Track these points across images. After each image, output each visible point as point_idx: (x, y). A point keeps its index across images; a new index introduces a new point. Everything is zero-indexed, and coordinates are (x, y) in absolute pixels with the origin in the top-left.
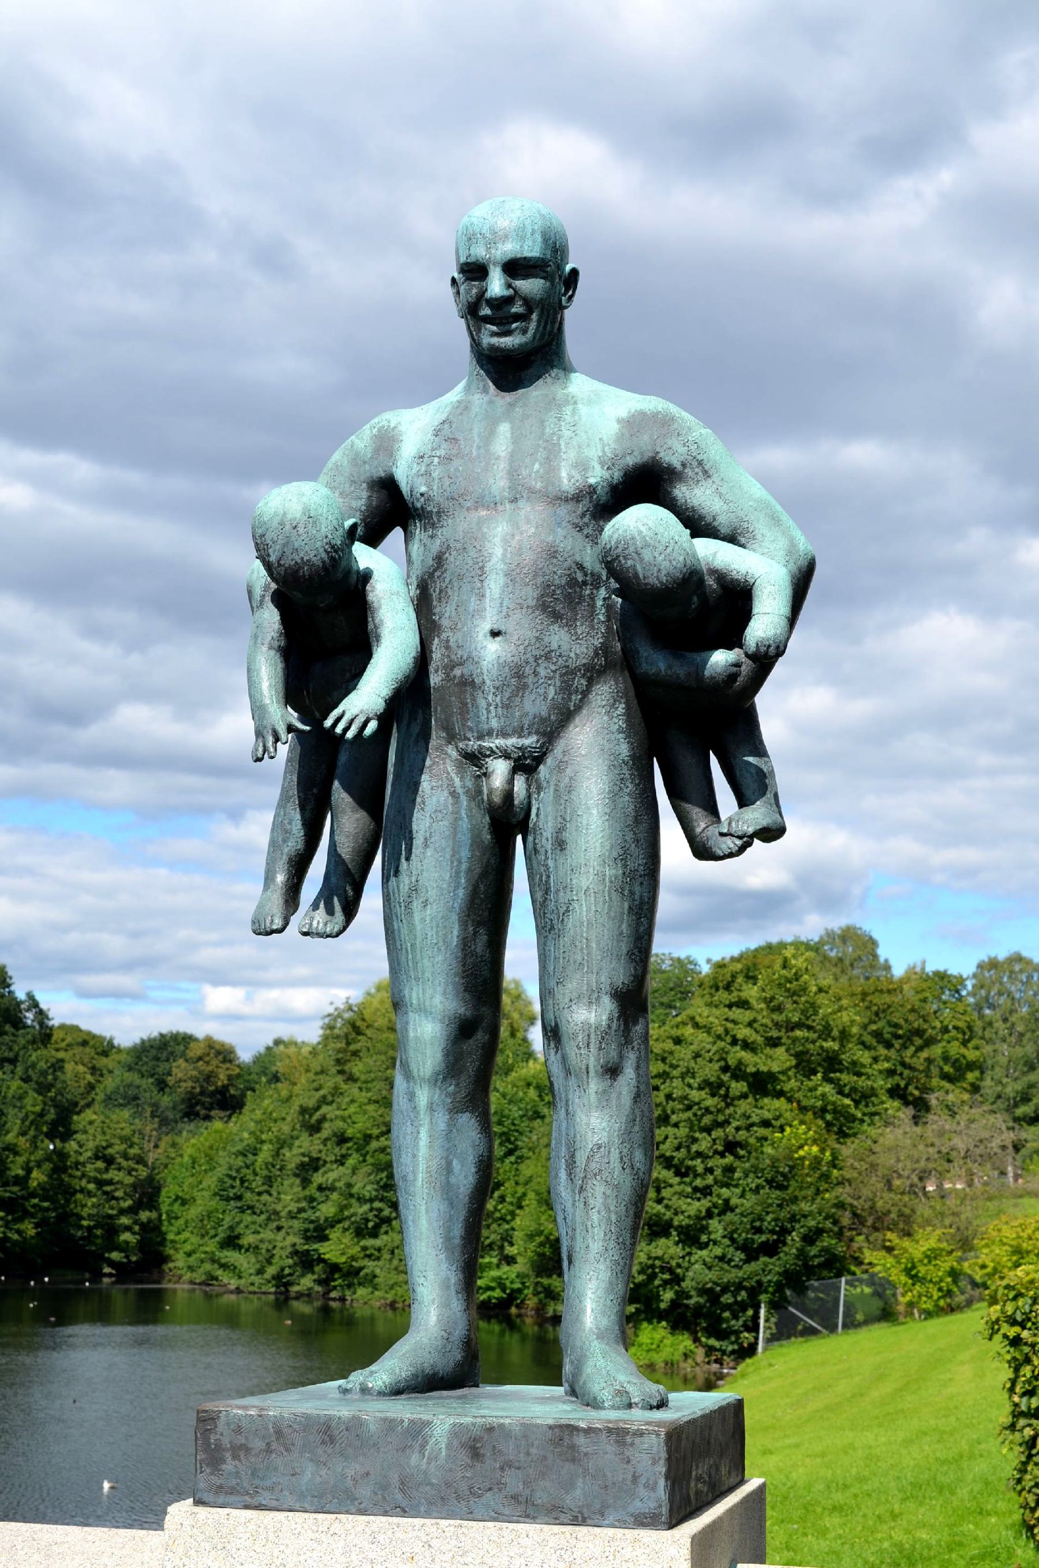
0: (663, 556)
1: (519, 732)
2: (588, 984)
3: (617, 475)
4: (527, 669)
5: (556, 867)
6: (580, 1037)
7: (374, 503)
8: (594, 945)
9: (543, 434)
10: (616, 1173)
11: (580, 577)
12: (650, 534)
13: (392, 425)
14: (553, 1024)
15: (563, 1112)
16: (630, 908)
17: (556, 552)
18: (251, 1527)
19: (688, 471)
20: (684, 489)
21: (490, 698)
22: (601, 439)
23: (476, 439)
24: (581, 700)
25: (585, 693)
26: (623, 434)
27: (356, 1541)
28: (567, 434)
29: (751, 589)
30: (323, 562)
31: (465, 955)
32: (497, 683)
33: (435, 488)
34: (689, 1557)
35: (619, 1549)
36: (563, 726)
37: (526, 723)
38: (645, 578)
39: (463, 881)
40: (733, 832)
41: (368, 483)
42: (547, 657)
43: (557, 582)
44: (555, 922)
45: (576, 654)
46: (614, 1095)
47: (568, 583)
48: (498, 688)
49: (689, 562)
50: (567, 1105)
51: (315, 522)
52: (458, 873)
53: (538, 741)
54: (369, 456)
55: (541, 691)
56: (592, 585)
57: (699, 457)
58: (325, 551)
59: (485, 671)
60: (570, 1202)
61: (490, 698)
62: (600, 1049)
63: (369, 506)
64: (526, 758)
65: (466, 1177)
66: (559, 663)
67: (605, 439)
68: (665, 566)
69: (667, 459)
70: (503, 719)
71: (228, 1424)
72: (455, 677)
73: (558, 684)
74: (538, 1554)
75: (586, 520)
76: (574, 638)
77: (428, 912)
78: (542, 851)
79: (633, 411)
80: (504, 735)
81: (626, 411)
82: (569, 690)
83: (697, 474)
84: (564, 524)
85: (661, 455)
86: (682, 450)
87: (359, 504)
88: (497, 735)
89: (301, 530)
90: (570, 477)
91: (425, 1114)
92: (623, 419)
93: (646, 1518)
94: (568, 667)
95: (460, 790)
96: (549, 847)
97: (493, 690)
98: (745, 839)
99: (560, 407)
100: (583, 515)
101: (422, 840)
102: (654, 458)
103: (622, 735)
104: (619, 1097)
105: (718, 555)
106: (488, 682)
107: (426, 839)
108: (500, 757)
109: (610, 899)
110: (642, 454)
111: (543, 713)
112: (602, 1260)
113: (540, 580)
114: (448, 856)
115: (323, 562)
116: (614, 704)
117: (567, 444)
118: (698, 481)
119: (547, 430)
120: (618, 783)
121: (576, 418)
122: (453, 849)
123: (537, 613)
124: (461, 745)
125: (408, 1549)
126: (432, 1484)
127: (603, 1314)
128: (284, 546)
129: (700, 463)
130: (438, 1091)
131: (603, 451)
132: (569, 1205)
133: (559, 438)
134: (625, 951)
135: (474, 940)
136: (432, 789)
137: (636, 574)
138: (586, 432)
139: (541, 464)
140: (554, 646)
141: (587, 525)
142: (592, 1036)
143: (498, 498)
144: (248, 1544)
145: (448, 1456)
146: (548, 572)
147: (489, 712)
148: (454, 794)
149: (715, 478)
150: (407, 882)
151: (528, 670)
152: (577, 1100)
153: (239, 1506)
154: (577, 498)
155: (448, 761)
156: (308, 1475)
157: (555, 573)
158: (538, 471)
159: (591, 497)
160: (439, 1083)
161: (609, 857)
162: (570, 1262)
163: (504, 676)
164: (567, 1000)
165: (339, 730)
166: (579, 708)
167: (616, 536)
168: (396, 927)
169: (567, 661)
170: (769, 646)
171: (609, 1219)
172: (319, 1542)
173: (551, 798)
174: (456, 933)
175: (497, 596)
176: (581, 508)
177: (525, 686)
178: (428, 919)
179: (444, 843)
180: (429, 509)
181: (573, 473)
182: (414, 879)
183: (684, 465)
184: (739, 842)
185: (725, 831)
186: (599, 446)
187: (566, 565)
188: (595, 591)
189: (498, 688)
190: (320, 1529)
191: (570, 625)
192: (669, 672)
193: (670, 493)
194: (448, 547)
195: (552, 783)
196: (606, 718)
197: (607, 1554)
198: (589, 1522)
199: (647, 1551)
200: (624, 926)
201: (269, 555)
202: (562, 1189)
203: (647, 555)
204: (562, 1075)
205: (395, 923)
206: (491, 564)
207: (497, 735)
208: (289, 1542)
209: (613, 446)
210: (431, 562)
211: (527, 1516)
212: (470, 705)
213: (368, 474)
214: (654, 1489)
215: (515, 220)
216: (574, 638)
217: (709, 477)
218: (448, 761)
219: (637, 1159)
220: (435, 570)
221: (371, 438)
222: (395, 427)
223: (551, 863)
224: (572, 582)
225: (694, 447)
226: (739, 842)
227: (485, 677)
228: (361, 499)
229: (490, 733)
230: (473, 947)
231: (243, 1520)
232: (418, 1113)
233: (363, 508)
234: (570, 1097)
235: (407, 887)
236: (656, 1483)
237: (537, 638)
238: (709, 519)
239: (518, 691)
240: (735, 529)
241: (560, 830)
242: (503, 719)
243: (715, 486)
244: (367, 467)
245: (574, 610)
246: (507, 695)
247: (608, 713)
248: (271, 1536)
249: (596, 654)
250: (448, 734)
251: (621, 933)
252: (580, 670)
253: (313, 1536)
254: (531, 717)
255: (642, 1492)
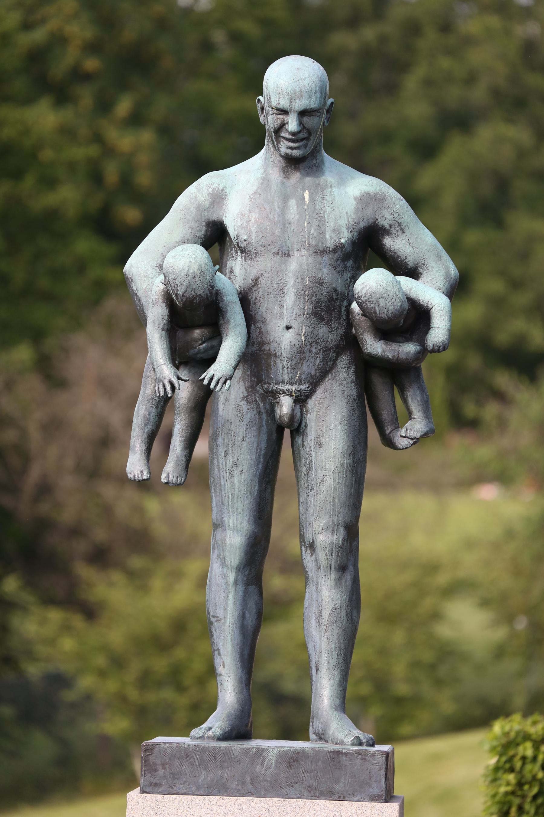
0: (390, 303)
1: (299, 382)
2: (333, 521)
3: (355, 235)
4: (306, 349)
5: (316, 457)
6: (328, 549)
7: (209, 234)
8: (336, 500)
9: (315, 209)
10: (344, 623)
11: (334, 296)
12: (384, 291)
13: (221, 188)
14: (311, 541)
15: (314, 589)
16: (356, 480)
17: (323, 282)
18: (176, 802)
19: (393, 230)
20: (390, 239)
21: (285, 363)
22: (346, 213)
23: (277, 209)
24: (333, 365)
25: (335, 361)
26: (358, 208)
27: (230, 809)
28: (328, 209)
29: (430, 311)
30: (207, 295)
31: (260, 500)
32: (289, 356)
33: (253, 238)
34: (398, 815)
35: (364, 811)
36: (322, 379)
37: (303, 377)
38: (380, 314)
39: (262, 460)
40: (408, 435)
41: (206, 223)
42: (317, 342)
43: (322, 300)
44: (314, 486)
45: (331, 339)
46: (343, 581)
47: (328, 300)
48: (289, 359)
49: (403, 305)
50: (317, 584)
51: (204, 274)
52: (259, 456)
53: (309, 387)
54: (208, 206)
55: (313, 361)
56: (340, 299)
57: (399, 221)
58: (209, 290)
59: (283, 349)
60: (318, 637)
61: (285, 363)
62: (338, 556)
63: (206, 235)
64: (301, 396)
65: (252, 621)
66: (322, 345)
67: (349, 212)
68: (391, 309)
69: (382, 223)
70: (290, 375)
71: (160, 752)
72: (265, 350)
73: (321, 356)
74: (323, 814)
75: (338, 262)
76: (330, 330)
77: (243, 477)
78: (308, 446)
79: (363, 192)
80: (291, 384)
81: (359, 192)
82: (327, 360)
83: (397, 231)
84: (327, 266)
85: (379, 221)
86: (389, 217)
87: (200, 234)
88: (287, 383)
89: (197, 279)
90: (331, 238)
91: (233, 586)
92: (357, 197)
93: (375, 797)
94: (326, 347)
95: (263, 411)
96: (312, 445)
97: (286, 359)
98: (415, 440)
99: (323, 190)
100: (337, 260)
101: (241, 437)
102: (374, 222)
103: (353, 384)
104: (346, 582)
105: (413, 289)
106: (284, 355)
107: (243, 437)
108: (288, 395)
109: (346, 476)
110: (368, 221)
111: (313, 372)
112: (336, 669)
113: (314, 299)
114: (255, 446)
115: (207, 295)
116: (349, 367)
117: (329, 216)
118: (398, 235)
119: (317, 207)
120: (352, 412)
121: (333, 197)
122: (258, 443)
123: (312, 317)
124: (265, 386)
125: (257, 812)
126: (267, 781)
127: (337, 697)
128: (187, 287)
129: (400, 225)
130: (240, 574)
131: (348, 221)
132: (317, 639)
133: (324, 212)
134: (352, 504)
135: (265, 492)
136: (248, 409)
137: (375, 312)
138: (338, 208)
139: (315, 230)
140: (320, 335)
141: (339, 265)
142: (334, 549)
143: (290, 248)
144: (174, 811)
145: (276, 766)
146: (318, 294)
147: (283, 370)
148: (260, 413)
149: (407, 233)
150: (231, 460)
151: (306, 349)
152: (323, 583)
153: (166, 793)
154: (334, 251)
155: (257, 395)
156: (202, 777)
157: (322, 294)
158: (313, 234)
159: (342, 250)
160: (241, 569)
161: (346, 453)
162: (317, 669)
163: (294, 352)
164: (320, 529)
165: (212, 386)
166: (331, 369)
167: (365, 290)
168: (222, 483)
169: (326, 344)
170: (440, 347)
171: (340, 647)
172: (211, 809)
173: (314, 418)
174: (257, 488)
175: (290, 307)
176: (336, 256)
177: (304, 358)
178: (242, 480)
179: (253, 439)
180: (249, 249)
181: (333, 235)
182: (235, 459)
183: (391, 226)
184: (411, 442)
185: (404, 435)
186: (346, 218)
187: (328, 290)
188: (341, 303)
189: (289, 359)
190: (212, 803)
191: (329, 323)
192: (383, 354)
193: (381, 241)
194: (262, 275)
195: (315, 410)
196: (345, 374)
197: (358, 813)
198: (347, 799)
199: (378, 812)
200: (352, 490)
201: (177, 290)
202: (313, 630)
203: (382, 303)
204: (314, 568)
205: (222, 481)
206: (287, 288)
207: (287, 383)
208: (195, 810)
209: (353, 217)
210: (251, 281)
211: (315, 796)
212: (272, 366)
213: (207, 217)
214: (379, 782)
215: (307, 85)
216: (330, 330)
217: (404, 232)
218: (257, 395)
219: (354, 615)
220: (253, 287)
221: (208, 195)
222: (223, 190)
223: (313, 453)
224: (331, 299)
225: (396, 215)
226: (411, 442)
227: (283, 352)
228: (201, 231)
229: (283, 382)
230: (264, 496)
231: (171, 799)
232: (228, 585)
233: (203, 236)
234: (320, 581)
235: (231, 463)
236: (380, 780)
237: (312, 332)
238: (403, 258)
239: (300, 360)
240: (417, 264)
241: (318, 437)
242: (290, 375)
243: (407, 238)
244: (206, 213)
245: (331, 315)
246: (294, 362)
247: (346, 372)
248: (186, 807)
249: (341, 339)
250: (258, 379)
251: (351, 494)
252: (333, 348)
253: (208, 806)
254: (306, 374)
255: (374, 785)
